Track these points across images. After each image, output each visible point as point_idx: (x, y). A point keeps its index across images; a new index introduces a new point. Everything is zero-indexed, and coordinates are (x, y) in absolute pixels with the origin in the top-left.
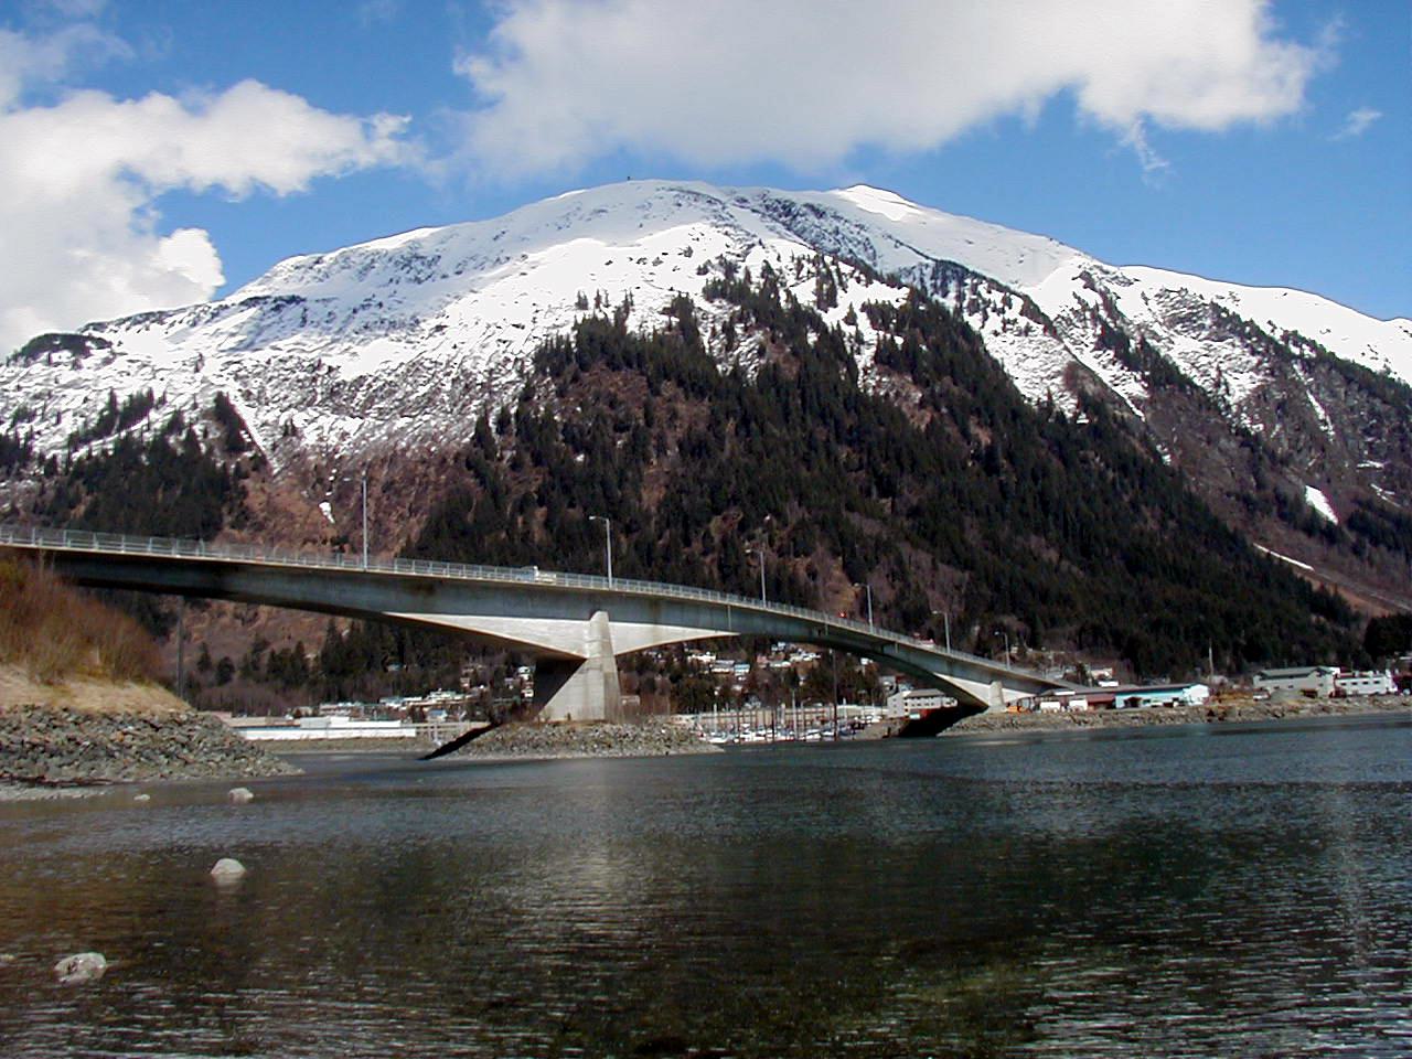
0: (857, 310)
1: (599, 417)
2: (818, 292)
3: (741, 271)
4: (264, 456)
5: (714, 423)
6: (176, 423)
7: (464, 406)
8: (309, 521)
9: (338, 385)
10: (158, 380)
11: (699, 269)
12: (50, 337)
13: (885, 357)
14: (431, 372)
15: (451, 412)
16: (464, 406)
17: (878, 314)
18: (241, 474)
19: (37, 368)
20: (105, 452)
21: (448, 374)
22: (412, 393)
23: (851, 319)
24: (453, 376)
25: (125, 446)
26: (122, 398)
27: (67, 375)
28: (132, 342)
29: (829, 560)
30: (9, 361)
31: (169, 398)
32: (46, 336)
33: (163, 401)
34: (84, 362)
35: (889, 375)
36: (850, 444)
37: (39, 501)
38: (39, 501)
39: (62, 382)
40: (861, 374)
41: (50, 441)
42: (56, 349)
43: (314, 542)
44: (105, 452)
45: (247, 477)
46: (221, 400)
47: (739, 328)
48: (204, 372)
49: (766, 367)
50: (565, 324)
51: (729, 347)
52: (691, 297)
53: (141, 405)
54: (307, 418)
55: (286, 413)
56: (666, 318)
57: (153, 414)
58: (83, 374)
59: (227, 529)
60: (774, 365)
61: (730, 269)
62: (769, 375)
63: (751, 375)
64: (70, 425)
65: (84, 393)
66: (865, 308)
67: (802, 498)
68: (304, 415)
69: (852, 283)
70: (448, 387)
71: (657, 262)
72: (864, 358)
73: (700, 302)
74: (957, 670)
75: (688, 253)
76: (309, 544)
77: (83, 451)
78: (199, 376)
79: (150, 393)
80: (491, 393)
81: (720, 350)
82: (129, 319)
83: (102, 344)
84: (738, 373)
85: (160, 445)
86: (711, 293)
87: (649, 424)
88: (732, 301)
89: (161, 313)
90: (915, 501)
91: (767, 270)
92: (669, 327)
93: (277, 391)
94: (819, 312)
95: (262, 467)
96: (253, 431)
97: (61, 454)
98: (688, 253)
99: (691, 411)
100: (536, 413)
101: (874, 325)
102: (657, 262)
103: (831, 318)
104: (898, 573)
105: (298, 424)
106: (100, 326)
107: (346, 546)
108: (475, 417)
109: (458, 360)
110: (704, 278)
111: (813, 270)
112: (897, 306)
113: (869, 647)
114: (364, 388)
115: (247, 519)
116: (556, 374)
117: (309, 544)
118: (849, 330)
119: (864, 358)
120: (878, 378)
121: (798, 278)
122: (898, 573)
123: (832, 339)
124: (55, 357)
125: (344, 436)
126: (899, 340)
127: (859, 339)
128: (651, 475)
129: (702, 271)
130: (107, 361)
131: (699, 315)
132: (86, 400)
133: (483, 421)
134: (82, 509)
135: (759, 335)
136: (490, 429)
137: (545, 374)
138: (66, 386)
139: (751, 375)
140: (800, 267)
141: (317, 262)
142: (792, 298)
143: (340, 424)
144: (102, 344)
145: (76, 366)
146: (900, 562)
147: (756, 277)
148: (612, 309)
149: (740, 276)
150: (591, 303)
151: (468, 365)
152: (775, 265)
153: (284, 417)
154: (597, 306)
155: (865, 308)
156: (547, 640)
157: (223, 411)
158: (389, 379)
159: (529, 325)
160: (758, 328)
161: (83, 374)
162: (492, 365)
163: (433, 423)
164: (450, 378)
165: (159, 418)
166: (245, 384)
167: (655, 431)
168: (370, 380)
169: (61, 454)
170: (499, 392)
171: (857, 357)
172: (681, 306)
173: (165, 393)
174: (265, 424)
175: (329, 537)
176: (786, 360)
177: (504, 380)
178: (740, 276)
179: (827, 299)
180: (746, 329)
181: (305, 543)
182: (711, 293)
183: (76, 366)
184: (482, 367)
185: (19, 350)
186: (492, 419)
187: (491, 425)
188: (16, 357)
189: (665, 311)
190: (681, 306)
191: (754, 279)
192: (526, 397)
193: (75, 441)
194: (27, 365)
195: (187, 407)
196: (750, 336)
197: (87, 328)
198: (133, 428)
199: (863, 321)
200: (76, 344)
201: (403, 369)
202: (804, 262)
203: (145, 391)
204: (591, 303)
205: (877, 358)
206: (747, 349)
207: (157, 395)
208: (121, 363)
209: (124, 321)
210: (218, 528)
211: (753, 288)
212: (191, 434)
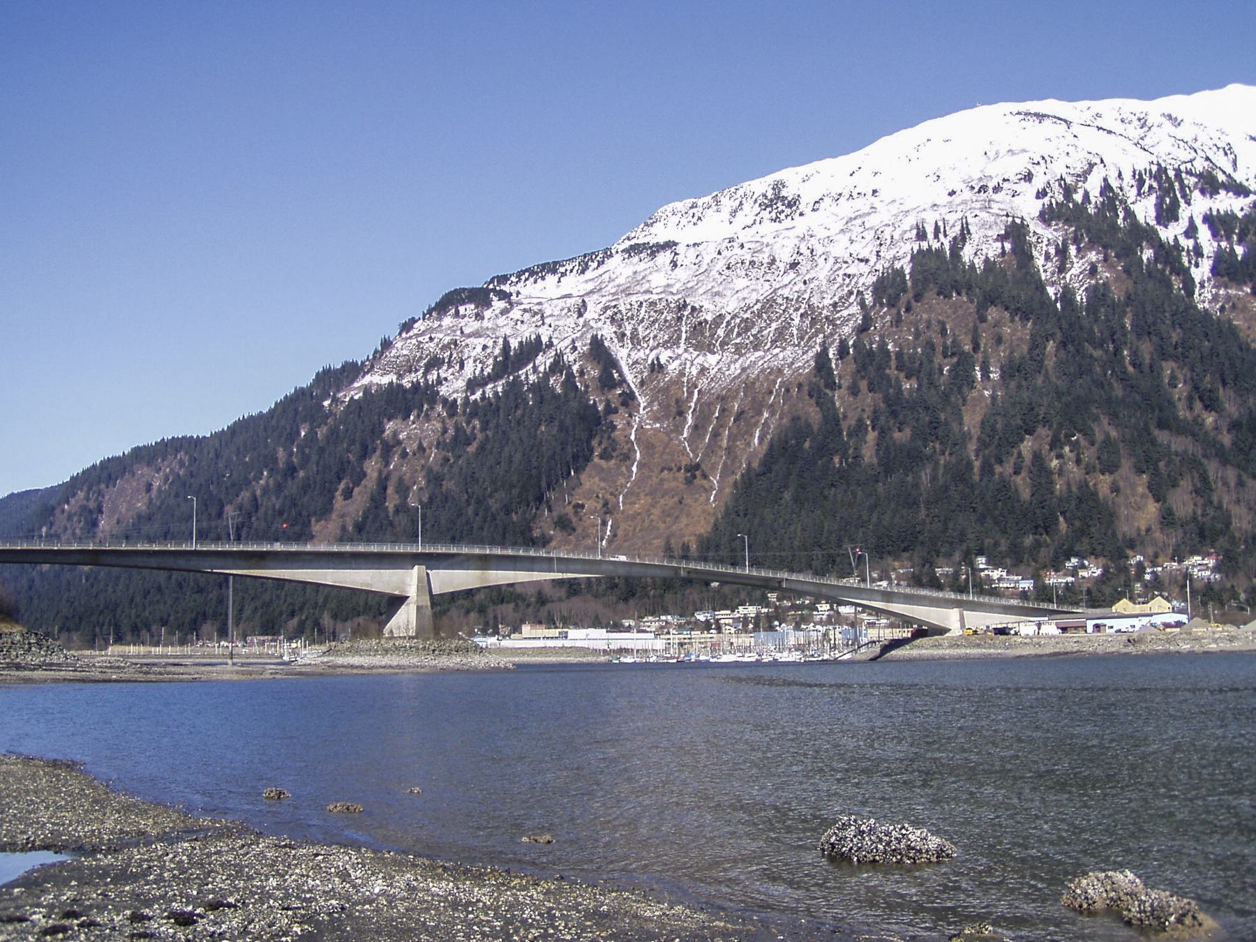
0: (1198, 221)
1: (930, 346)
2: (1159, 206)
3: (1081, 192)
4: (632, 393)
5: (1036, 344)
6: (558, 365)
7: (810, 338)
8: (667, 450)
9: (700, 323)
10: (546, 327)
11: (1038, 192)
12: (457, 292)
13: (1224, 269)
14: (783, 308)
15: (798, 345)
16: (810, 338)
17: (1219, 224)
18: (609, 410)
19: (448, 321)
20: (496, 393)
21: (797, 310)
22: (766, 328)
23: (1191, 232)
24: (802, 311)
25: (515, 386)
26: (514, 344)
27: (471, 325)
28: (529, 291)
29: (1133, 477)
30: (424, 315)
31: (555, 341)
32: (456, 290)
33: (550, 345)
34: (487, 314)
35: (1226, 287)
36: (1175, 358)
37: (441, 439)
38: (441, 439)
39: (467, 331)
40: (1198, 286)
41: (453, 387)
42: (463, 303)
43: (670, 469)
44: (496, 393)
45: (616, 412)
46: (597, 344)
47: (1073, 250)
48: (587, 315)
49: (1096, 287)
50: (902, 255)
51: (1062, 269)
52: (1028, 221)
53: (533, 348)
54: (672, 355)
55: (655, 352)
56: (999, 244)
57: (540, 359)
58: (486, 323)
59: (596, 460)
60: (1104, 284)
61: (1068, 191)
62: (1098, 295)
63: (1081, 296)
64: (470, 370)
65: (482, 341)
66: (1208, 219)
67: (1114, 416)
68: (669, 353)
69: (1196, 194)
70: (797, 321)
71: (997, 189)
72: (1201, 272)
73: (1035, 227)
74: (864, 595)
75: (1028, 177)
76: (666, 472)
77: (478, 395)
78: (581, 321)
79: (538, 337)
80: (834, 325)
81: (1053, 274)
82: (526, 270)
83: (504, 296)
84: (1067, 295)
85: (541, 388)
86: (1047, 216)
87: (976, 348)
88: (1067, 221)
89: (555, 263)
90: (1236, 415)
91: (1106, 188)
92: (1003, 253)
93: (648, 331)
94: (1158, 227)
95: (630, 402)
96: (625, 370)
97: (459, 397)
98: (1028, 177)
99: (1017, 332)
100: (871, 344)
101: (1215, 235)
102: (997, 189)
103: (1167, 234)
104: (1203, 489)
105: (663, 361)
106: (503, 279)
107: (697, 473)
108: (818, 348)
109: (806, 296)
110: (1040, 202)
111: (1155, 185)
112: (1240, 215)
113: (762, 583)
114: (724, 324)
115: (614, 450)
116: (891, 305)
117: (666, 472)
118: (1188, 244)
119: (1201, 272)
120: (1214, 291)
121: (1139, 194)
122: (1203, 489)
123: (1168, 254)
124: (462, 309)
125: (703, 370)
126: (1239, 250)
127: (1198, 251)
128: (974, 398)
129: (1041, 194)
130: (504, 312)
131: (1034, 239)
132: (485, 347)
133: (825, 351)
134: (475, 445)
135: (1093, 256)
136: (830, 360)
137: (882, 305)
138: (469, 336)
139: (1081, 296)
140: (1141, 182)
141: (692, 207)
142: (1130, 214)
143: (700, 360)
144: (504, 296)
145: (479, 317)
146: (1204, 478)
147: (1095, 193)
148: (949, 238)
149: (1078, 197)
150: (930, 236)
151: (814, 301)
152: (1114, 184)
153: (653, 356)
154: (936, 236)
155: (1208, 219)
156: (368, 585)
157: (598, 351)
158: (746, 316)
159: (873, 259)
160: (1091, 249)
161: (486, 323)
162: (836, 299)
163: (781, 356)
164: (799, 313)
165: (543, 361)
166: (620, 327)
167: (979, 356)
168: (728, 318)
169: (459, 397)
170: (842, 324)
171: (1193, 270)
172: (1016, 233)
173: (551, 338)
174: (636, 362)
175: (683, 464)
176: (1117, 279)
177: (845, 313)
178: (1078, 197)
179: (1167, 214)
180: (1079, 250)
181: (662, 471)
182: (1047, 216)
183: (479, 317)
184: (827, 302)
185: (433, 305)
186: (832, 353)
187: (831, 356)
188: (430, 312)
189: (1001, 238)
190: (1016, 233)
191: (1093, 200)
192: (862, 329)
193: (472, 385)
194: (440, 319)
195: (568, 350)
196: (1081, 258)
197: (492, 281)
198: (520, 372)
199: (1204, 233)
200: (480, 297)
201: (759, 306)
202: (1146, 177)
203: (533, 337)
204: (930, 236)
205: (1215, 270)
206: (1080, 270)
207: (545, 339)
208: (516, 313)
209: (523, 272)
210: (588, 459)
211: (1091, 210)
212: (570, 376)
